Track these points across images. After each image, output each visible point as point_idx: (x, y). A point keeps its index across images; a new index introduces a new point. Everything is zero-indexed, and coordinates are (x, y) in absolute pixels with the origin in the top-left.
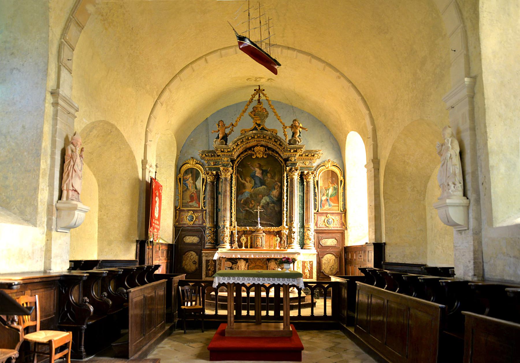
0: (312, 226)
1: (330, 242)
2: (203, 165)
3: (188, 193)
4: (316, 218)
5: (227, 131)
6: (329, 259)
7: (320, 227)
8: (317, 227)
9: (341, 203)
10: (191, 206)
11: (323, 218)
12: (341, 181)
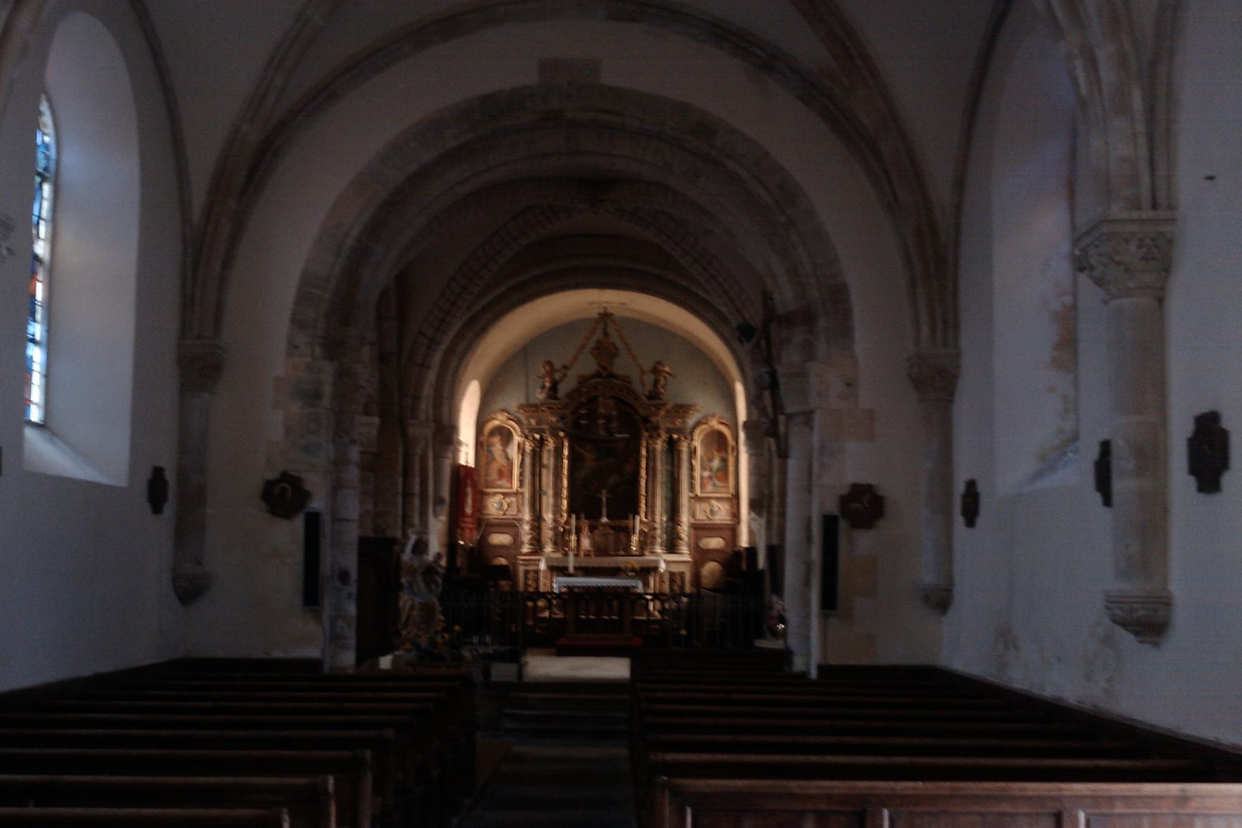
0: (685, 518)
1: (715, 543)
2: (518, 422)
3: (495, 467)
5: (557, 376)
6: (711, 568)
10: (500, 487)
11: (705, 506)
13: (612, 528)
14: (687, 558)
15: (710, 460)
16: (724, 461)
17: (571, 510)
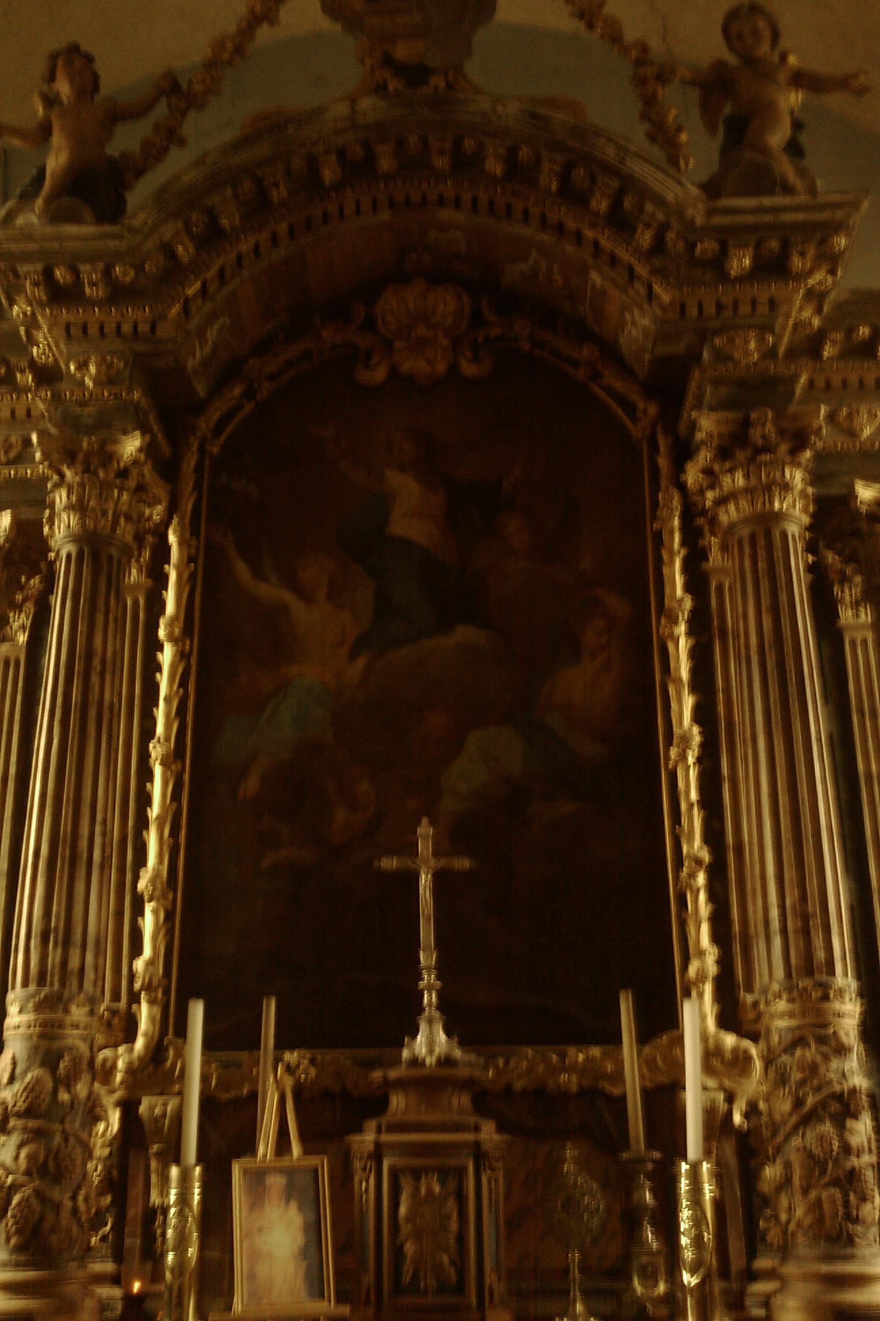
13: (485, 1101)
17: (191, 969)
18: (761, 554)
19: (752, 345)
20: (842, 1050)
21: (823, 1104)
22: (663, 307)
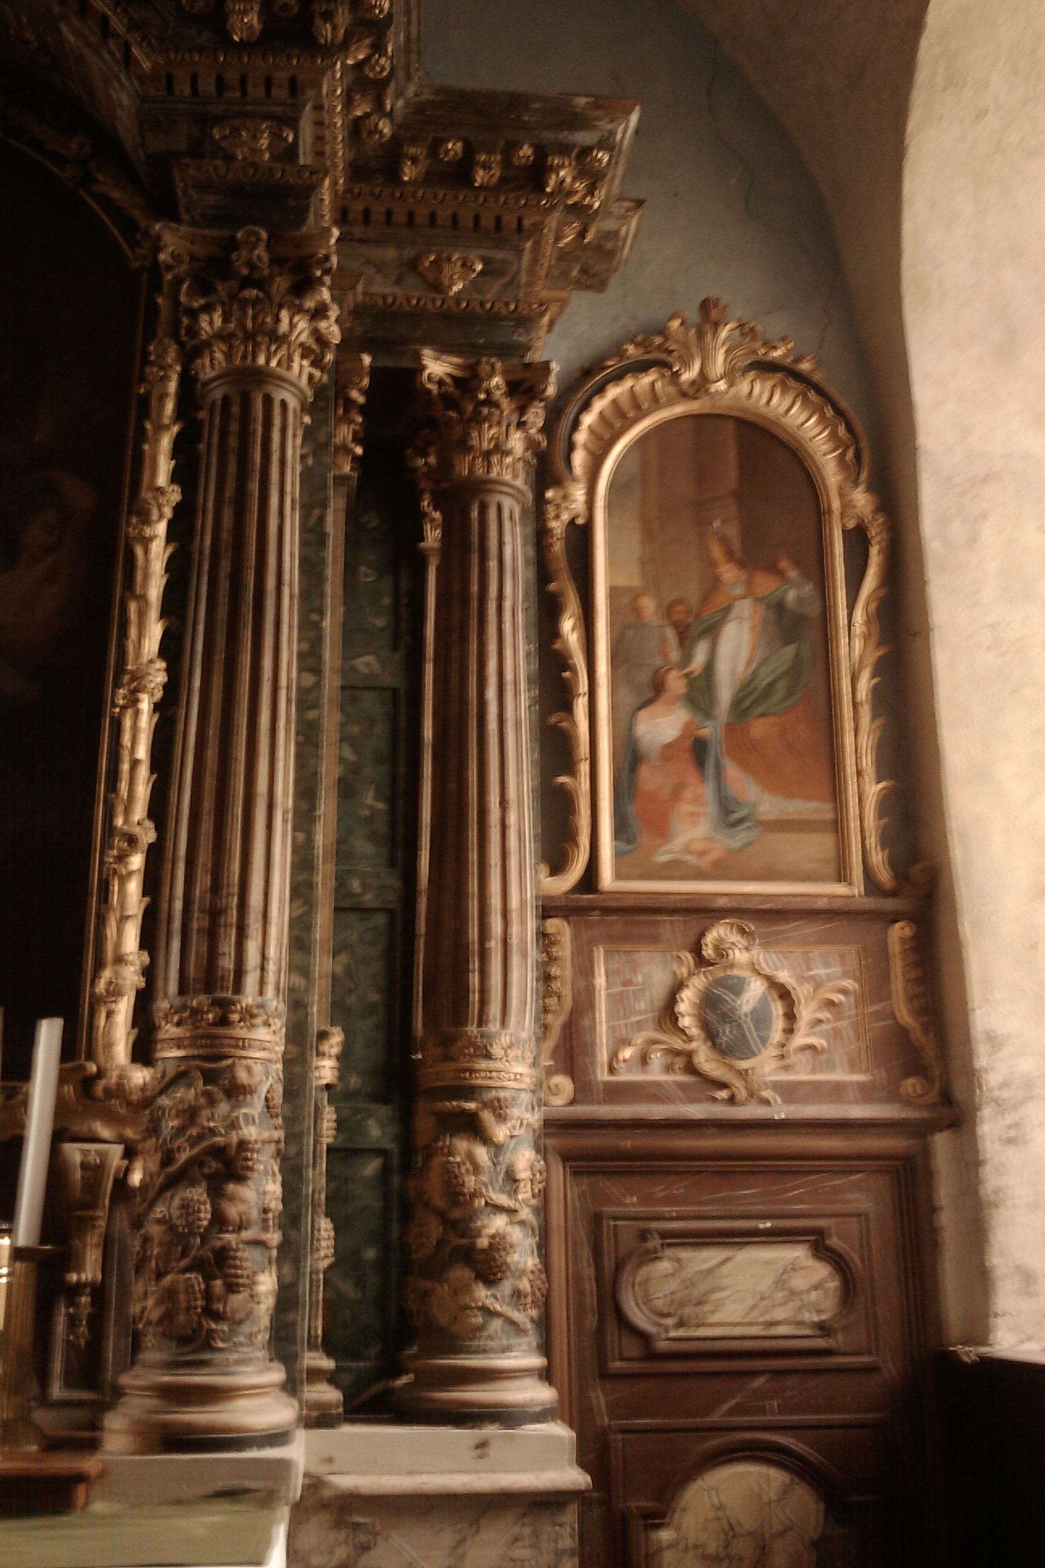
0: (515, 1066)
1: (755, 1290)
4: (564, 971)
7: (617, 1092)
8: (583, 1091)
9: (866, 790)
11: (654, 971)
12: (858, 540)
14: (544, 1458)
15: (696, 626)
16: (802, 632)
18: (234, 426)
19: (264, 142)
20: (236, 1092)
21: (195, 1162)
22: (142, 79)
